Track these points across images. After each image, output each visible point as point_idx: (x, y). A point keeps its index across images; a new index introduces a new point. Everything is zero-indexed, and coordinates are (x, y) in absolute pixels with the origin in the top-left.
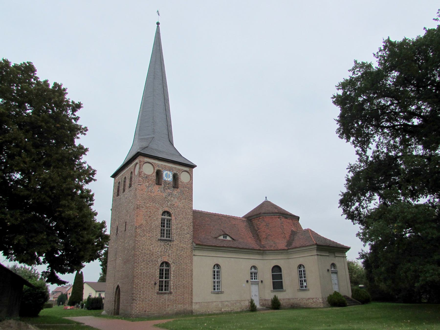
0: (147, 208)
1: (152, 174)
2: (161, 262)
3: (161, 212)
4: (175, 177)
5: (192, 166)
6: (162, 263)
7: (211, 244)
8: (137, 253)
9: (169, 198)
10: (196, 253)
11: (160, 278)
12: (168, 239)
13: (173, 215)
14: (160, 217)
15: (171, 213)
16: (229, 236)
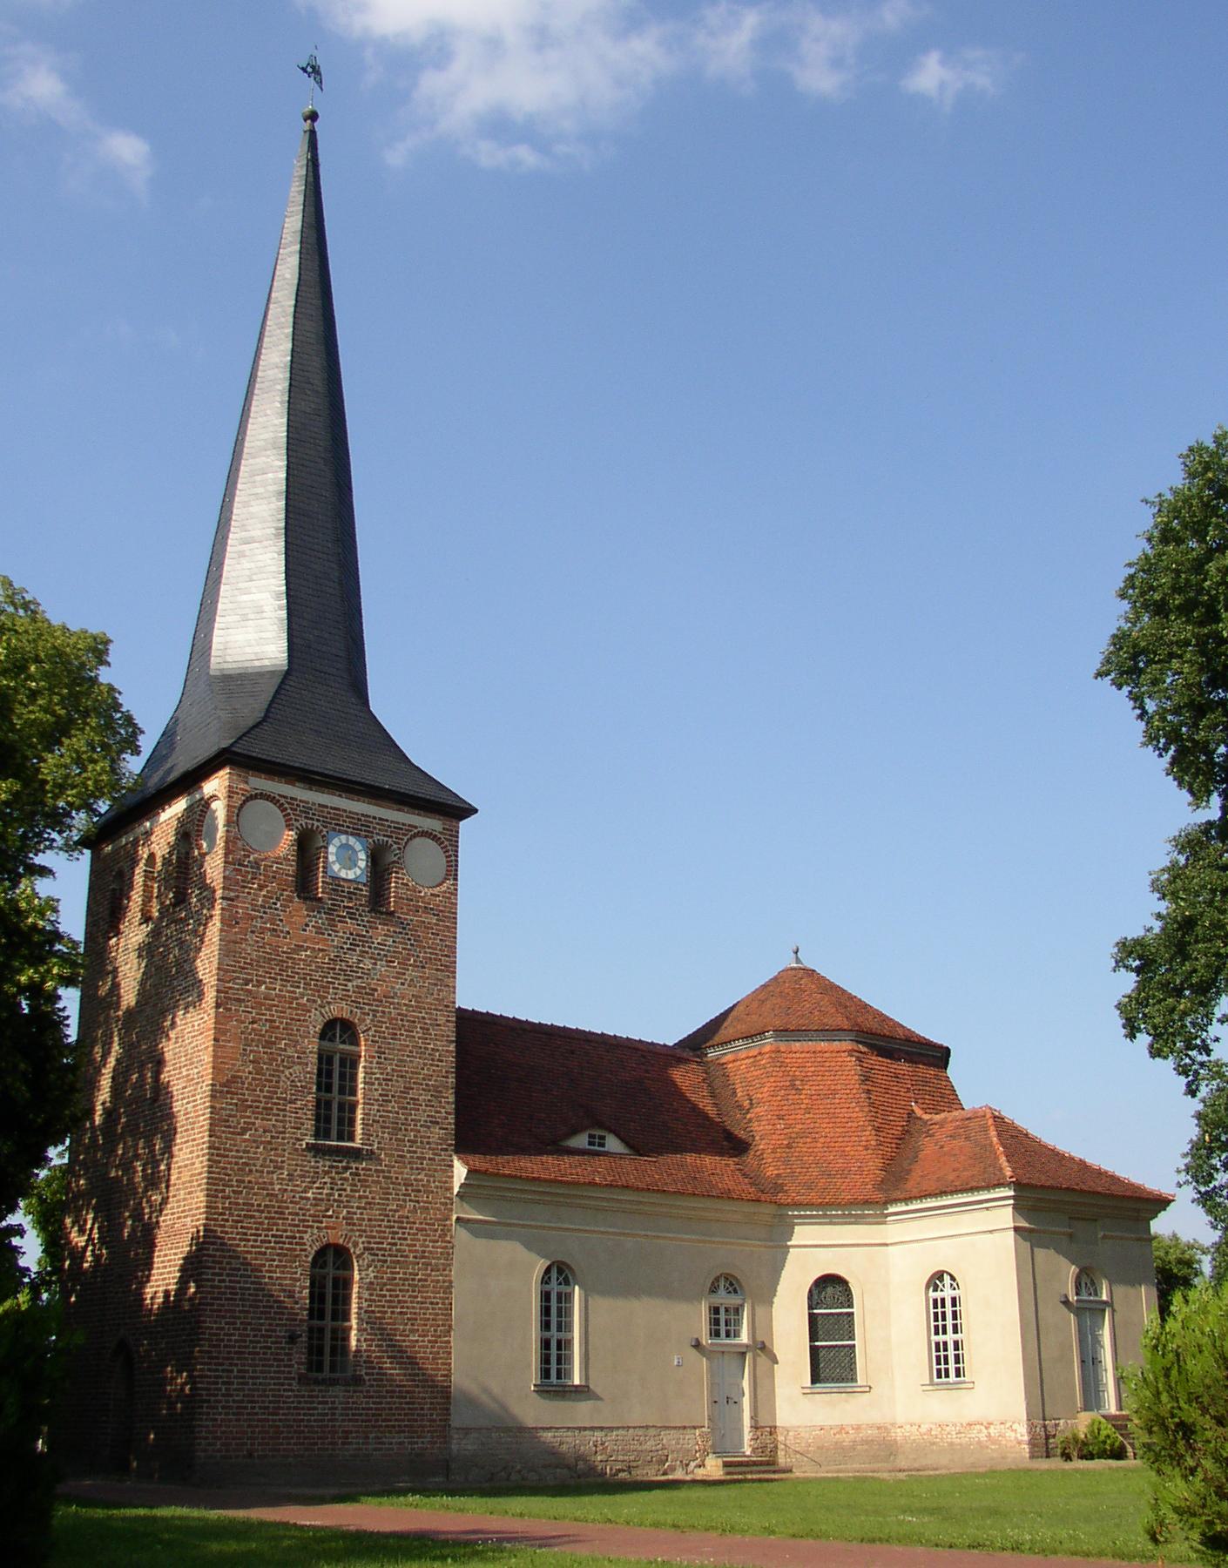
4: (377, 858)
5: (467, 811)
6: (321, 1253)
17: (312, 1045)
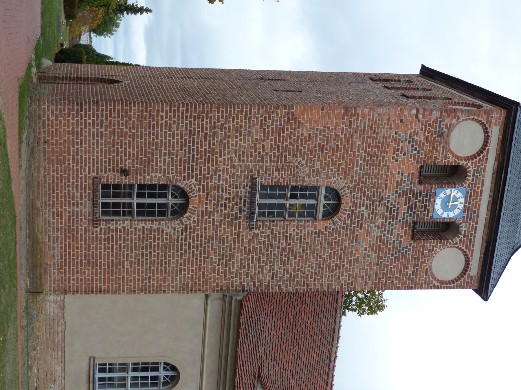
5: (484, 290)
6: (183, 194)
17: (322, 182)
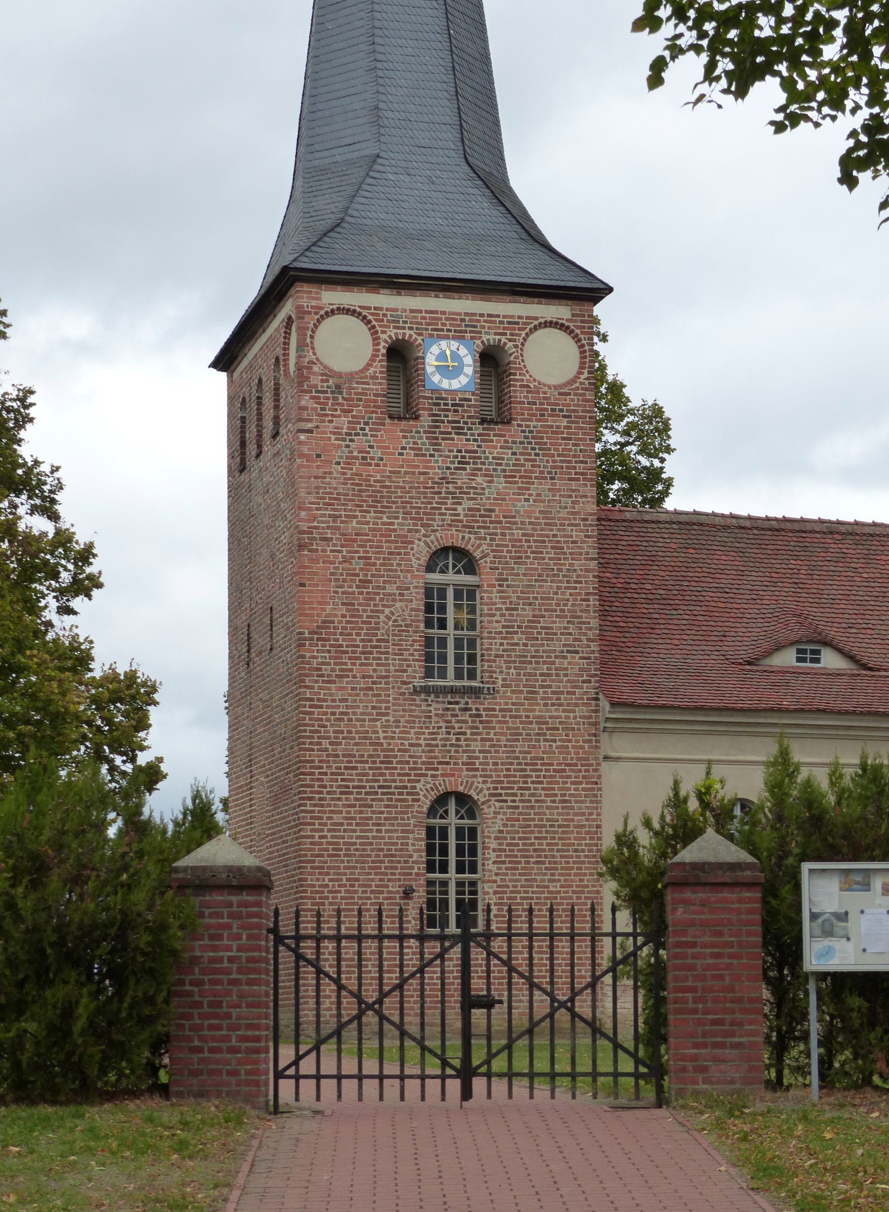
0: (348, 541)
1: (366, 368)
2: (433, 795)
3: (420, 551)
4: (491, 361)
5: (597, 291)
6: (441, 800)
7: (703, 695)
8: (315, 756)
9: (462, 478)
10: (619, 745)
11: (473, 884)
12: (466, 683)
13: (485, 564)
14: (417, 580)
15: (477, 554)
16: (840, 651)
